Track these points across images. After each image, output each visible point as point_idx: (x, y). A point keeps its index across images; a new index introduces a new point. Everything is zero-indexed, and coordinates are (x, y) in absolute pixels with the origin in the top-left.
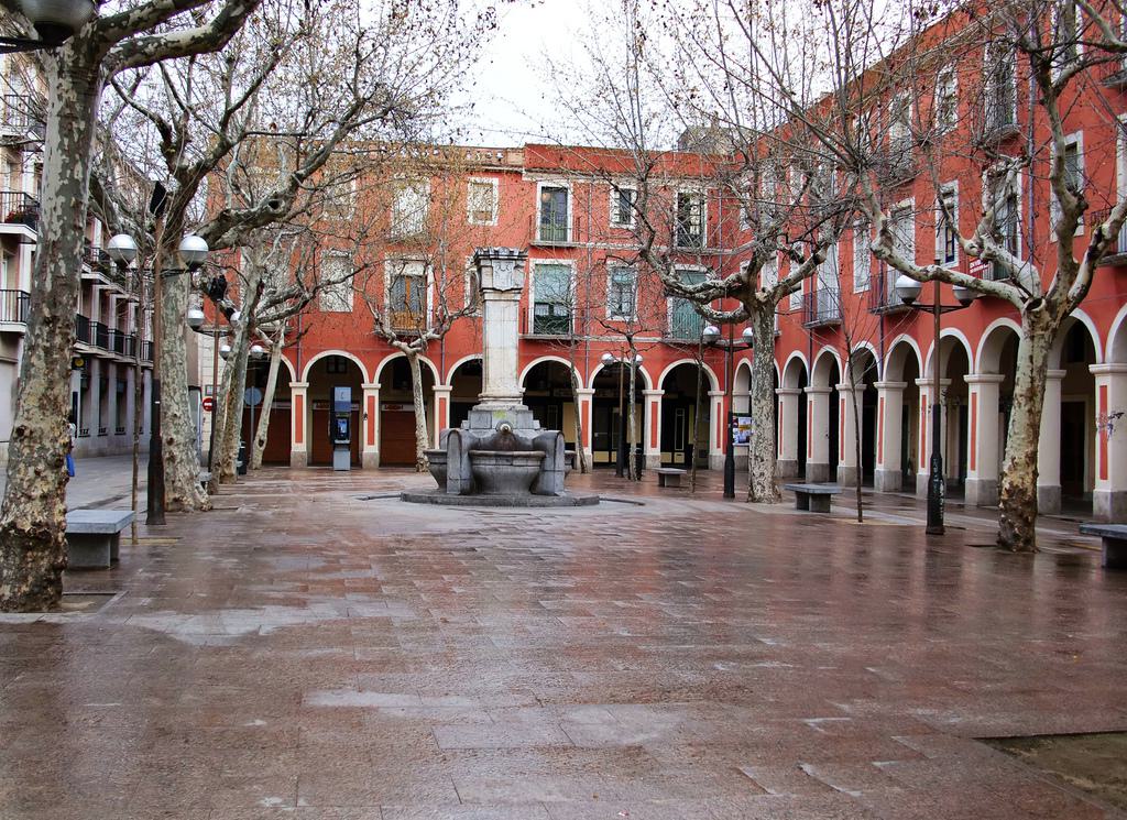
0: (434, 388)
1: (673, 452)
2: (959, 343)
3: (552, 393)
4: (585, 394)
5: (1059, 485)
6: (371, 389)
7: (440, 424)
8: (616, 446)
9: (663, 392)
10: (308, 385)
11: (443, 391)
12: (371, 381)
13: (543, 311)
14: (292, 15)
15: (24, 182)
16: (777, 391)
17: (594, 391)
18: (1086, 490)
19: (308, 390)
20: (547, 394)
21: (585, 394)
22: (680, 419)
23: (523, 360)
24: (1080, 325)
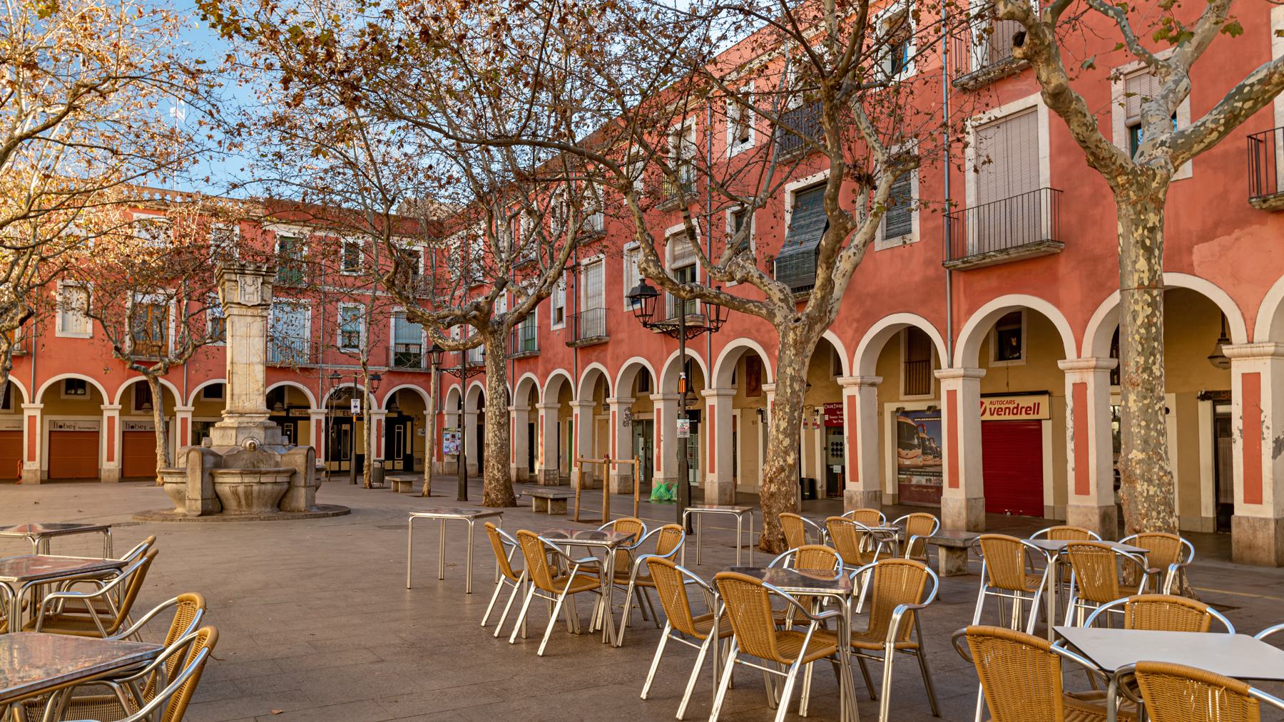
0: (175, 409)
1: (394, 460)
2: (602, 374)
3: (288, 414)
4: (318, 413)
5: (982, 495)
6: (111, 409)
7: (1197, 486)
8: (399, 455)
9: (120, 407)
10: (42, 406)
11: (184, 411)
12: (111, 403)
13: (402, 349)
14: (766, 23)
15: (1011, 30)
16: (509, 408)
17: (120, 407)
18: (1049, 499)
19: (193, 412)
20: (283, 414)
21: (318, 413)
22: (399, 434)
23: (267, 383)
24: (692, 359)
